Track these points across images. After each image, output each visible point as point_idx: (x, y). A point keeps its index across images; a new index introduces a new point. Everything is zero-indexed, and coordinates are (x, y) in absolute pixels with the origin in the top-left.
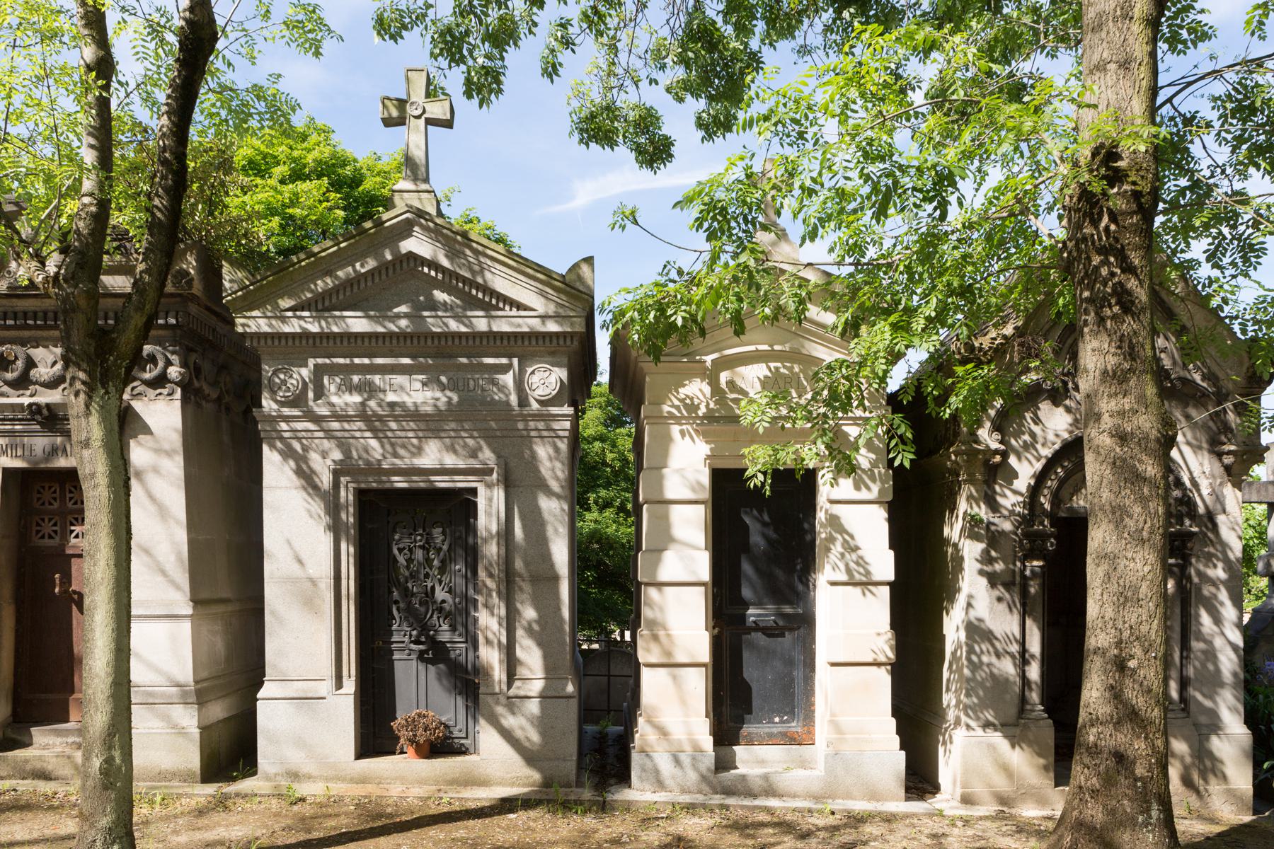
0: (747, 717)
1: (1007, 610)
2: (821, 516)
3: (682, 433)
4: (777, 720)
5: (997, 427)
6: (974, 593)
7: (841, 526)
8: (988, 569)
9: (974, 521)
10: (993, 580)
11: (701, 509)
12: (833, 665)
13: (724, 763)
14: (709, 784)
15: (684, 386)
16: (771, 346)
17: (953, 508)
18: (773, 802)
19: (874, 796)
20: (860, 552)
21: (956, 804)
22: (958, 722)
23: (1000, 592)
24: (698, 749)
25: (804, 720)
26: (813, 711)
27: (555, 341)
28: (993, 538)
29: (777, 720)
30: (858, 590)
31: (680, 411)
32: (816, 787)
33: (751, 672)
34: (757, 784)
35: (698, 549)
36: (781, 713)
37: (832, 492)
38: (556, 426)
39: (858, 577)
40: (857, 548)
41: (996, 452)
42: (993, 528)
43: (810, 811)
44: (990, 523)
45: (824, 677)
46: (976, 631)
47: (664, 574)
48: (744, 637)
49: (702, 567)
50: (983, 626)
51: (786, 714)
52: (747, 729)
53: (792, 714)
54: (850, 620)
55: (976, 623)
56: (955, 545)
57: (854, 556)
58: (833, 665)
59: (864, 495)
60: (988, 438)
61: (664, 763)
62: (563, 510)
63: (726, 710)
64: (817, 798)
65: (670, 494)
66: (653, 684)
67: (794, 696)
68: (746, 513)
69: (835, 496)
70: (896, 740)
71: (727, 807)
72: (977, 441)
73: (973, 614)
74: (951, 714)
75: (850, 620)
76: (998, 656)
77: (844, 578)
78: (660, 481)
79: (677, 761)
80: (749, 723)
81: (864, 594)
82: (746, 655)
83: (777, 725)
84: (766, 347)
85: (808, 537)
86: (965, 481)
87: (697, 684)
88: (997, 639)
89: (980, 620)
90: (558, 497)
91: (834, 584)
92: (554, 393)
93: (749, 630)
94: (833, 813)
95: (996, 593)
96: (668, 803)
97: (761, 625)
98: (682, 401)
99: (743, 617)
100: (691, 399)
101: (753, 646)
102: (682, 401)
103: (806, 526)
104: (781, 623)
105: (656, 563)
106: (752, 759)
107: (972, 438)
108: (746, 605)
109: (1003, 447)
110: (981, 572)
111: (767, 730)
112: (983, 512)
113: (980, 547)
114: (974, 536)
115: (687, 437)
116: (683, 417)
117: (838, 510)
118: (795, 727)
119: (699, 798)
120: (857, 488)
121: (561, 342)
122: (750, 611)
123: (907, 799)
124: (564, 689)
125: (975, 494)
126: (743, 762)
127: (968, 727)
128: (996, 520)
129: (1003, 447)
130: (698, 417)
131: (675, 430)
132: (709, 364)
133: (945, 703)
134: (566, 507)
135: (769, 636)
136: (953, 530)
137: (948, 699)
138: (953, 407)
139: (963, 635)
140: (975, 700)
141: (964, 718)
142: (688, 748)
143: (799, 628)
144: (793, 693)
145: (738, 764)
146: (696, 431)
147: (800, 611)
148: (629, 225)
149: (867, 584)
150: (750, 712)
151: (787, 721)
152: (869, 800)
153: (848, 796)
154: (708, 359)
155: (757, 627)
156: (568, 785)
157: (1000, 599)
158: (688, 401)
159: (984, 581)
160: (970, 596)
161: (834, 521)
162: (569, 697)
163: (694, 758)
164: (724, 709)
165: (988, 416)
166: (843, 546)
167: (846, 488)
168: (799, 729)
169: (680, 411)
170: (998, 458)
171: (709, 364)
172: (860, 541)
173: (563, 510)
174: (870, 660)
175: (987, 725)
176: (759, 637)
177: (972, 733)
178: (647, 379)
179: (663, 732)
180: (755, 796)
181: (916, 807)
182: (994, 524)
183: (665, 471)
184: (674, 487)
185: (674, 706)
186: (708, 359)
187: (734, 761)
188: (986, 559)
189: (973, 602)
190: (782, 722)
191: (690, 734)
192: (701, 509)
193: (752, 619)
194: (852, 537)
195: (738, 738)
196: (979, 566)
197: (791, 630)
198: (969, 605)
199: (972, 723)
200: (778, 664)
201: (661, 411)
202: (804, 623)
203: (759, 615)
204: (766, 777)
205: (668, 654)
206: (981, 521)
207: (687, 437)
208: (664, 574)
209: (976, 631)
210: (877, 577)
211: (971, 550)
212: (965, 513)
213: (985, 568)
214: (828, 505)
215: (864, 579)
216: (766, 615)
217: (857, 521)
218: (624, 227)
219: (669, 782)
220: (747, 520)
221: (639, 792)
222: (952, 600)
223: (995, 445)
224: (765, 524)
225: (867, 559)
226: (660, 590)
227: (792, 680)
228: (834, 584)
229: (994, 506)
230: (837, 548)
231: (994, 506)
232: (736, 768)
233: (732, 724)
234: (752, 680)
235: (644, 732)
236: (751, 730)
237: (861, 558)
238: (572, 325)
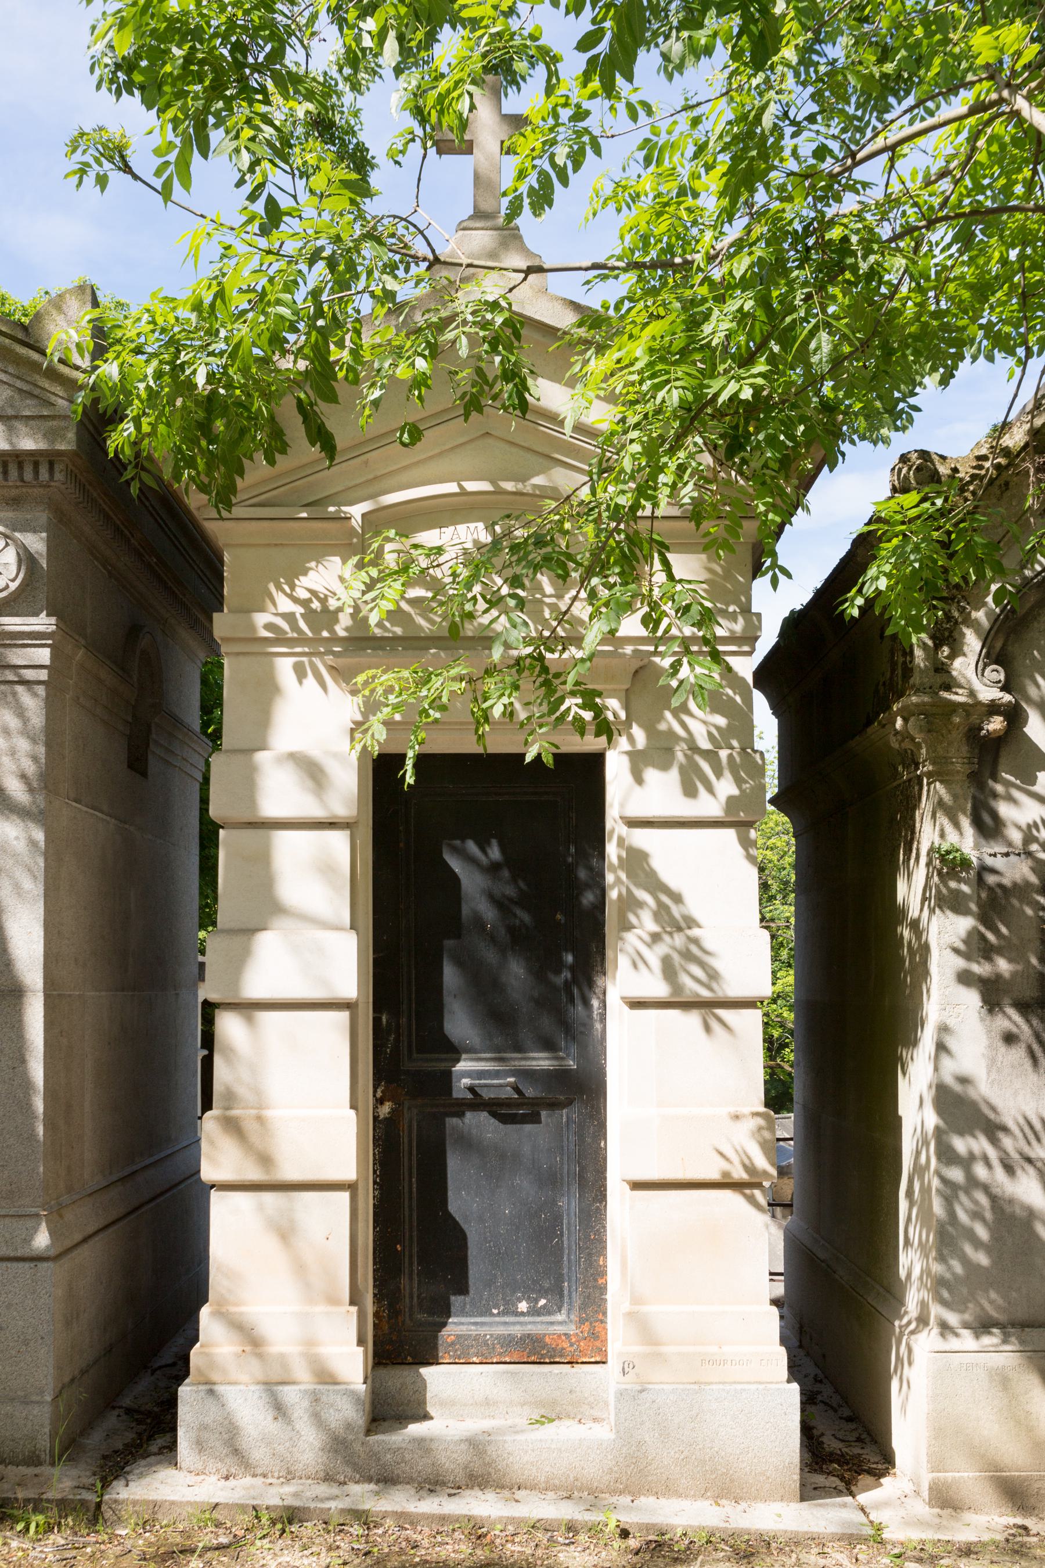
0: (456, 1300)
1: (1028, 1063)
2: (612, 850)
3: (300, 672)
4: (523, 1306)
5: (996, 654)
6: (951, 1022)
7: (652, 874)
8: (979, 969)
9: (949, 864)
10: (992, 994)
11: (339, 843)
12: (637, 1186)
13: (390, 1408)
14: (351, 1461)
15: (305, 572)
16: (493, 482)
17: (905, 832)
18: (481, 1505)
19: (726, 1489)
20: (695, 932)
21: (922, 1509)
22: (923, 1320)
23: (1013, 1019)
24: (326, 1377)
25: (583, 1307)
26: (603, 1289)
27: (13, 473)
28: (993, 903)
29: (523, 1306)
30: (692, 1020)
31: (294, 627)
32: (594, 1469)
33: (465, 1199)
34: (452, 1461)
35: (338, 928)
36: (532, 1291)
37: (632, 794)
38: (17, 657)
39: (692, 988)
40: (691, 922)
41: (993, 708)
42: (991, 879)
43: (572, 1528)
44: (985, 869)
45: (623, 1212)
46: (958, 1107)
47: (257, 984)
48: (452, 1122)
49: (341, 964)
50: (972, 1093)
51: (543, 1293)
52: (457, 1327)
53: (557, 1293)
54: (681, 1081)
55: (957, 1088)
56: (915, 925)
57: (679, 940)
58: (637, 1186)
59: (709, 806)
60: (973, 676)
61: (245, 1405)
62: (33, 843)
63: (409, 1285)
64: (592, 1495)
65: (270, 807)
66: (234, 1231)
67: (563, 1255)
68: (455, 850)
69: (636, 811)
70: (780, 1356)
71: (362, 1517)
72: (949, 685)
73: (949, 1067)
74: (913, 1299)
75: (681, 1081)
76: (1009, 1169)
77: (660, 989)
78: (248, 783)
79: (279, 1409)
80: (463, 1313)
81: (708, 1028)
82: (453, 1163)
83: (523, 1320)
84: (484, 486)
85: (588, 898)
86: (929, 774)
87: (332, 1229)
88: (1005, 1129)
89: (964, 1080)
90: (23, 813)
91: (637, 1004)
92: (13, 586)
93: (460, 1108)
94: (625, 1534)
95: (1002, 1023)
96: (242, 1508)
97: (486, 1094)
98: (305, 603)
99: (446, 1078)
100: (323, 601)
101: (468, 1144)
102: (305, 603)
103: (582, 874)
104: (530, 1092)
105: (240, 959)
106: (462, 1396)
107: (939, 679)
108: (454, 1052)
109: (1007, 698)
110: (965, 978)
111: (501, 1330)
112: (965, 841)
113: (963, 924)
114: (954, 903)
115: (310, 680)
116: (302, 640)
117: (642, 839)
118: (560, 1325)
119: (311, 1493)
120: (690, 791)
121: (28, 475)
122: (463, 1066)
123: (808, 1493)
124: (28, 1240)
125: (947, 798)
126: (443, 1404)
127: (945, 1328)
128: (998, 863)
129: (1007, 698)
130: (335, 639)
131: (285, 667)
132: (356, 522)
133: (903, 1274)
134: (39, 836)
135: (506, 1119)
136: (911, 889)
137: (911, 1262)
138: (869, 590)
139: (932, 1119)
140: (958, 1268)
141: (936, 1310)
142: (302, 1373)
143: (569, 1103)
144: (560, 1247)
145: (431, 1409)
146: (331, 669)
147: (572, 1064)
148: (117, 178)
149: (709, 1006)
150: (463, 1289)
151: (546, 1311)
152: (717, 1500)
153: (667, 1489)
154: (356, 511)
155: (477, 1101)
156: (33, 1460)
157: (1009, 1039)
158: (316, 605)
159: (972, 999)
160: (944, 1029)
161: (637, 861)
162: (38, 1259)
163: (316, 1399)
164: (404, 1281)
165: (975, 625)
166: (657, 916)
167: (661, 792)
168: (572, 1329)
169: (294, 627)
170: (996, 724)
171: (356, 522)
172: (694, 906)
173: (33, 843)
174: (715, 1176)
175: (982, 1326)
176: (479, 1124)
177: (954, 1343)
178: (227, 558)
179: (252, 1339)
180: (456, 1489)
181: (829, 1516)
182: (993, 871)
183: (262, 757)
184: (279, 793)
185: (281, 1277)
186: (356, 511)
187: (423, 1402)
188: (977, 947)
189: (951, 1042)
190: (534, 1311)
191: (310, 1343)
192: (339, 843)
193: (466, 1081)
194: (677, 898)
195: (435, 1348)
196: (961, 963)
197: (553, 1105)
198: (941, 1047)
199: (953, 1319)
200: (524, 1184)
201: (252, 627)
202: (582, 1091)
203: (481, 1074)
204: (476, 1444)
205: (265, 1160)
206: (965, 863)
207: (310, 680)
208: (257, 984)
209: (958, 1107)
210: (733, 990)
211: (945, 933)
212: (931, 850)
213: (976, 968)
214: (622, 830)
215: (705, 993)
216: (497, 1074)
217: (699, 871)
218: (102, 181)
219: (258, 1454)
220: (456, 865)
221: (180, 1487)
222: (913, 1042)
223: (988, 694)
224: (493, 869)
225: (708, 945)
226: (250, 1020)
227: (557, 1219)
228: (637, 1004)
229: (989, 826)
230: (647, 922)
231: (989, 826)
232: (426, 1417)
233: (422, 1317)
234: (453, 1227)
235: (214, 1339)
236: (462, 1330)
237: (696, 941)
238: (51, 435)
